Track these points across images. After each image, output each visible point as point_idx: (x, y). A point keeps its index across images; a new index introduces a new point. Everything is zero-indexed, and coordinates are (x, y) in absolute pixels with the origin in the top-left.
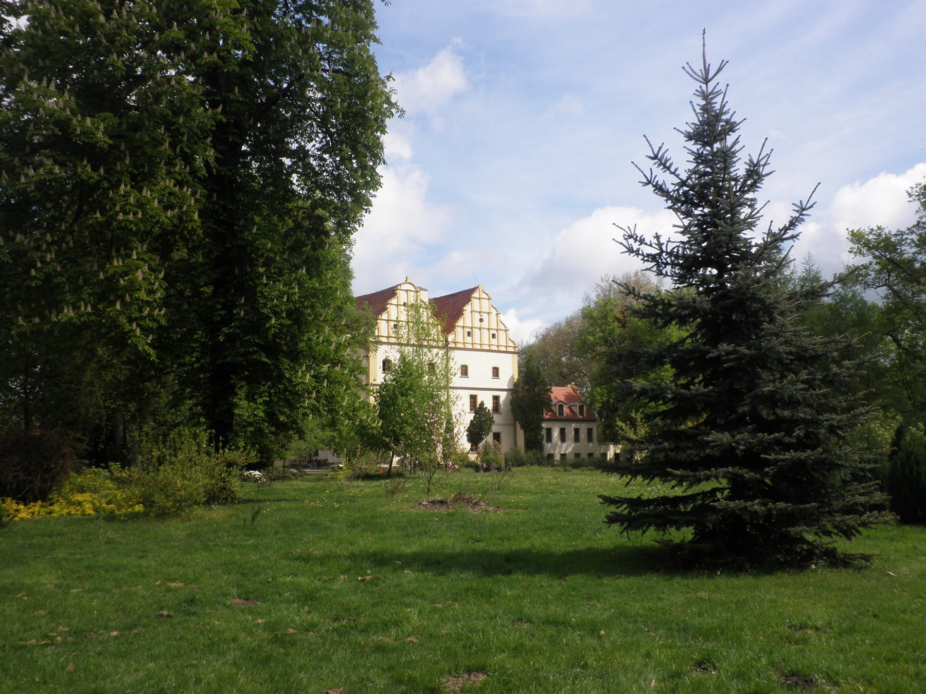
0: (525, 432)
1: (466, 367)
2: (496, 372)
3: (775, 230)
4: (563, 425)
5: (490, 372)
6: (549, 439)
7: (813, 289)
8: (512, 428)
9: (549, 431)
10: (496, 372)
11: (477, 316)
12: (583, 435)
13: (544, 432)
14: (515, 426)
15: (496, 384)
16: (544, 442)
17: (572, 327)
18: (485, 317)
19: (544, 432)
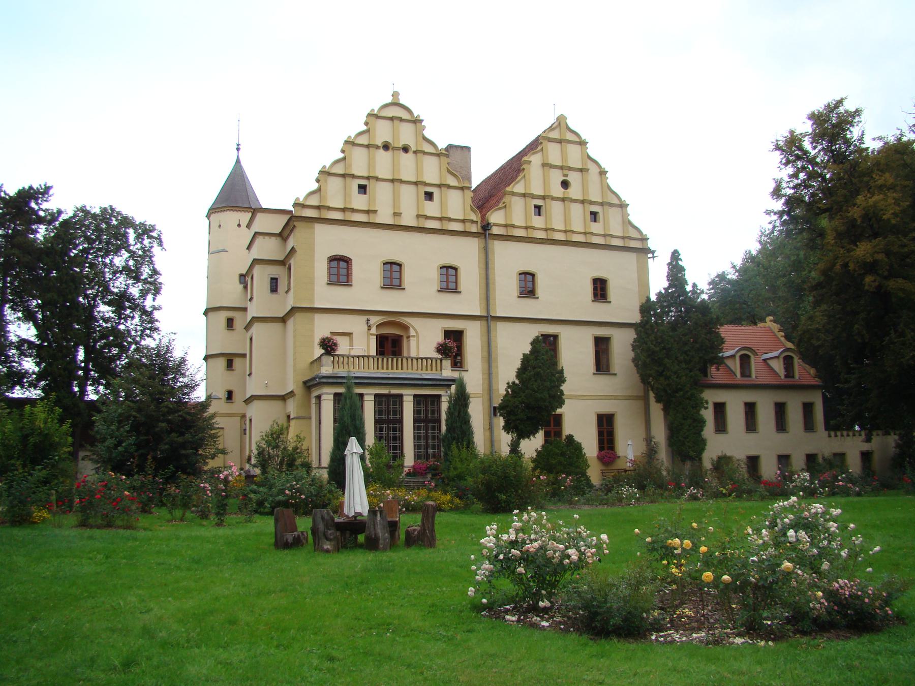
0: (666, 410)
1: (276, 279)
2: (600, 289)
3: (280, 187)
4: (780, 397)
5: (588, 289)
6: (721, 426)
7: (760, 252)
8: (640, 404)
9: (720, 409)
10: (600, 289)
11: (556, 177)
12: (795, 415)
13: (708, 414)
14: (646, 399)
15: (600, 312)
16: (709, 431)
17: (870, 226)
18: (573, 177)
19: (708, 414)
